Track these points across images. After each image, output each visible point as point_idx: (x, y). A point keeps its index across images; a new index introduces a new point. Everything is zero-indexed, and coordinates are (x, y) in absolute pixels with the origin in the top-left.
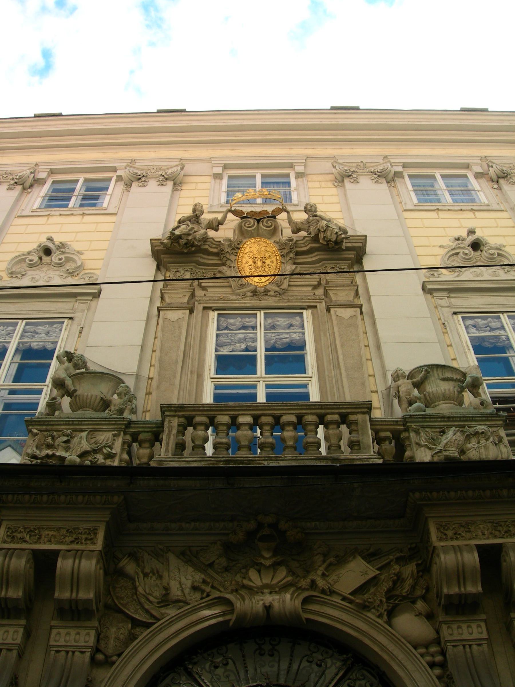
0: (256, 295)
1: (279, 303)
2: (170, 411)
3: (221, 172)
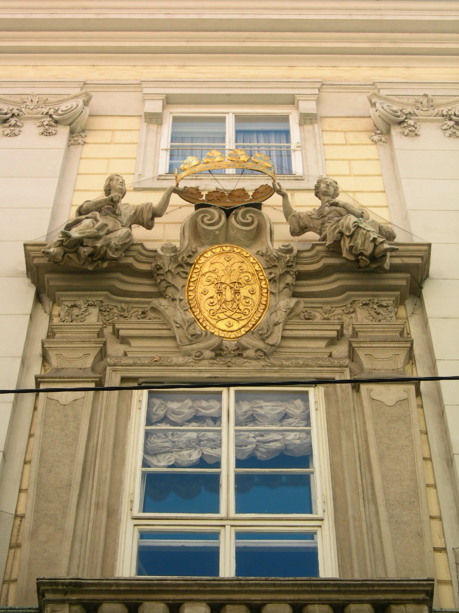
0: (220, 355)
1: (264, 371)
2: (55, 591)
3: (159, 110)
